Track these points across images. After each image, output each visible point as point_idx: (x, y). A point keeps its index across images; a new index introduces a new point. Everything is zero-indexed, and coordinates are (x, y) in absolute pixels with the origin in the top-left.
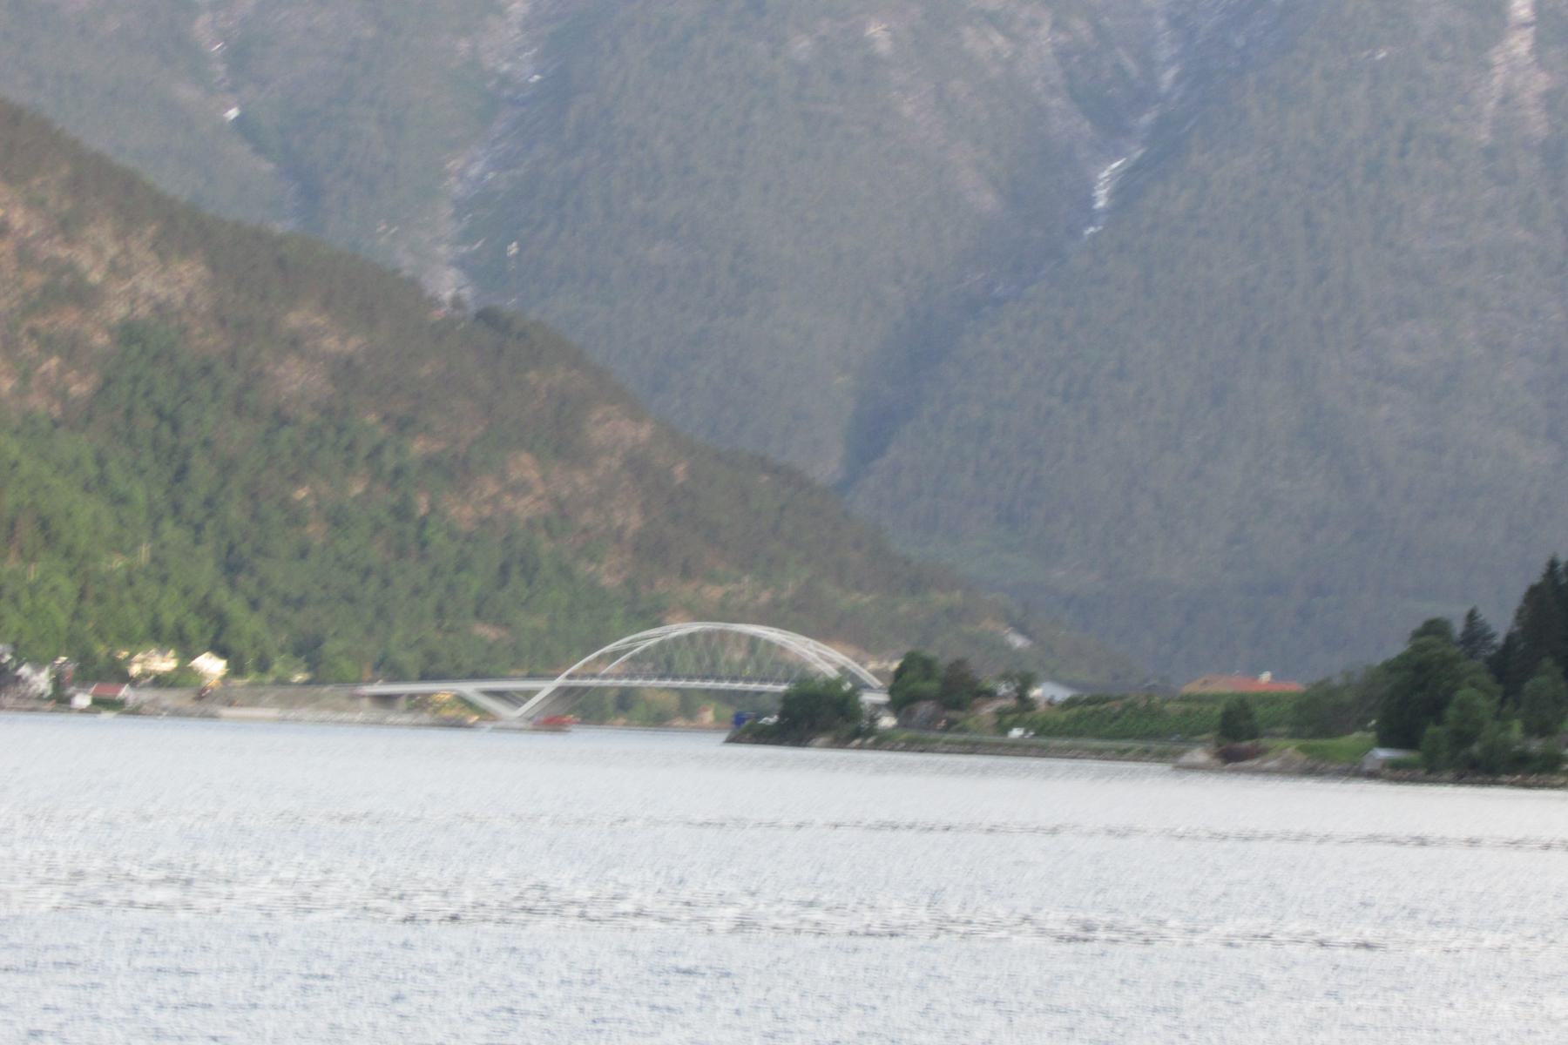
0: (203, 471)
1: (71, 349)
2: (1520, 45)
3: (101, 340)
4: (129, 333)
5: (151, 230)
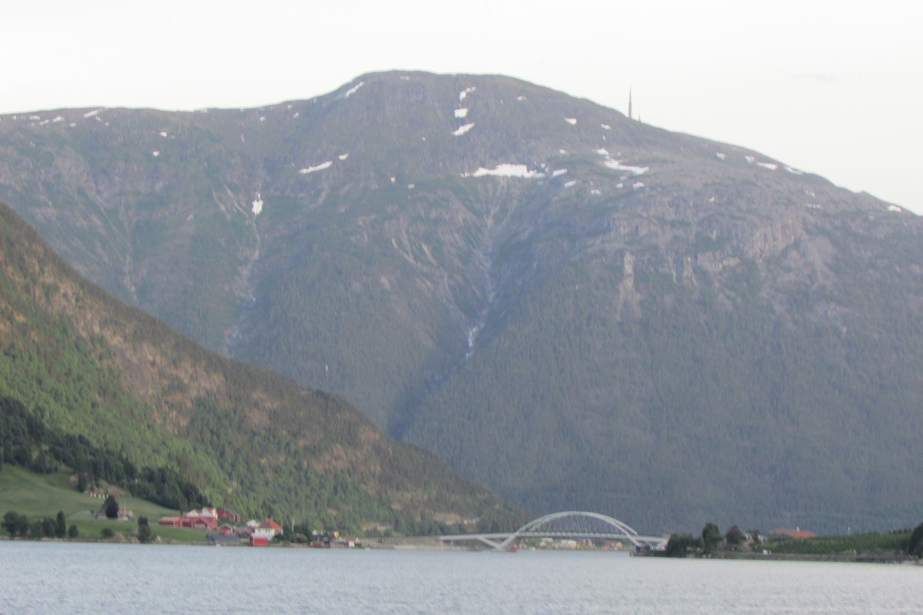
0: (229, 452)
1: (180, 408)
2: (629, 283)
3: (189, 405)
4: (199, 402)
5: (204, 363)
